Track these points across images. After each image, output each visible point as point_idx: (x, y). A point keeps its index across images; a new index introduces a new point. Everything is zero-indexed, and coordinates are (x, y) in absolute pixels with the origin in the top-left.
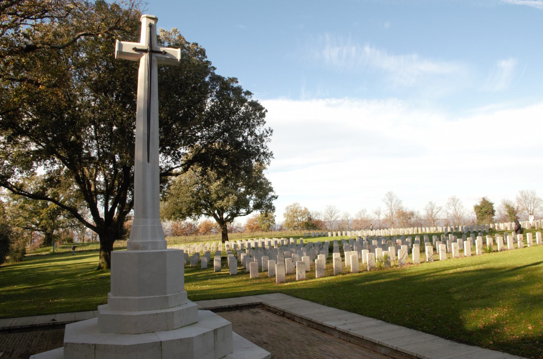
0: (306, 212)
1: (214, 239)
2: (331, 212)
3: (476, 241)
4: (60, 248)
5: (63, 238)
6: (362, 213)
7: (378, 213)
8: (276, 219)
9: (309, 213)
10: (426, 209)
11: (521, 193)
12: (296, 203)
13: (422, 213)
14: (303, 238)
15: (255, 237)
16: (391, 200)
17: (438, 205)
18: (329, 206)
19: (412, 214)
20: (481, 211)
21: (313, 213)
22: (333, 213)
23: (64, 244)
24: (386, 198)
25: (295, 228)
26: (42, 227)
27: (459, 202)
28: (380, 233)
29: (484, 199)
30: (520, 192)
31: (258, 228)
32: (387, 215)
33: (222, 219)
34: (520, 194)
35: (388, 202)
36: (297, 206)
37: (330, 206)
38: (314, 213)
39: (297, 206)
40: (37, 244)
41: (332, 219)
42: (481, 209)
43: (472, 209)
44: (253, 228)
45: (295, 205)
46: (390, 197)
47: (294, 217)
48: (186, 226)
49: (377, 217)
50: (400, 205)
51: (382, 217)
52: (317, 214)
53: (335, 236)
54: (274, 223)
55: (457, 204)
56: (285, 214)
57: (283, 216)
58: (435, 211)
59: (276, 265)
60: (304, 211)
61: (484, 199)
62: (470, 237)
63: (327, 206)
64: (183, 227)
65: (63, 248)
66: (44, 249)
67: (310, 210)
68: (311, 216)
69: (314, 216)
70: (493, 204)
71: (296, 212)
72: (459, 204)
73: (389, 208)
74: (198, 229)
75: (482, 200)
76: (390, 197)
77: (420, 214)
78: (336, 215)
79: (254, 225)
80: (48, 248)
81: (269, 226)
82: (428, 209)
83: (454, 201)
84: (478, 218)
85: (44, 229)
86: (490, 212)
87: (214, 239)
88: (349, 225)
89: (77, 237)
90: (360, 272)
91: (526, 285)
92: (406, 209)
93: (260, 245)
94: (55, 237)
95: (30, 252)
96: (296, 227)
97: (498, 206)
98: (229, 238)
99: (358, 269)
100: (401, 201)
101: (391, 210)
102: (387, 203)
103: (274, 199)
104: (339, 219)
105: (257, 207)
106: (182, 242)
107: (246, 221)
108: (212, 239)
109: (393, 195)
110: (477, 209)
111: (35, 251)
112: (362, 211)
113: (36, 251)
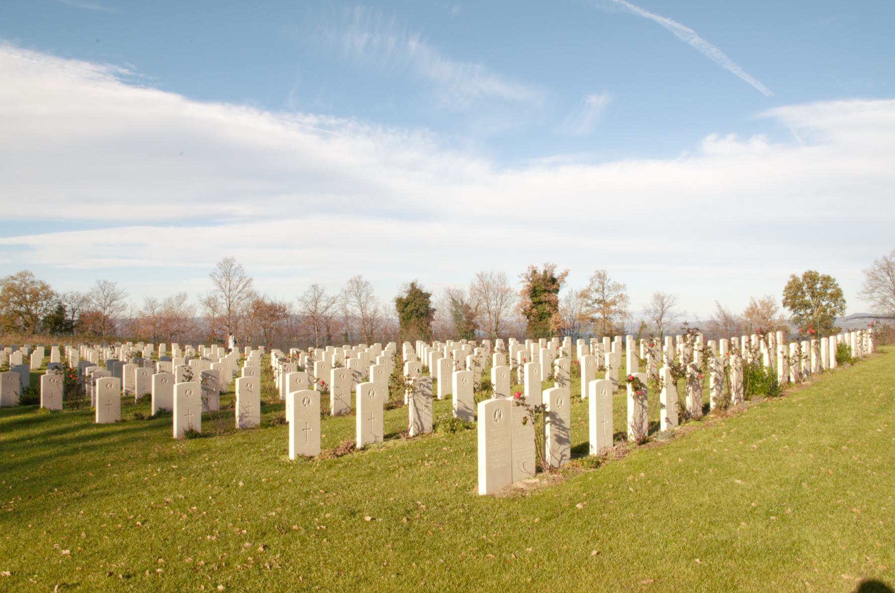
11: (481, 277)
14: (731, 387)
16: (228, 275)
20: (405, 309)
29: (413, 285)
30: (478, 276)
34: (478, 279)
43: (393, 306)
59: (153, 376)
75: (409, 288)
77: (293, 309)
83: (358, 287)
97: (438, 301)
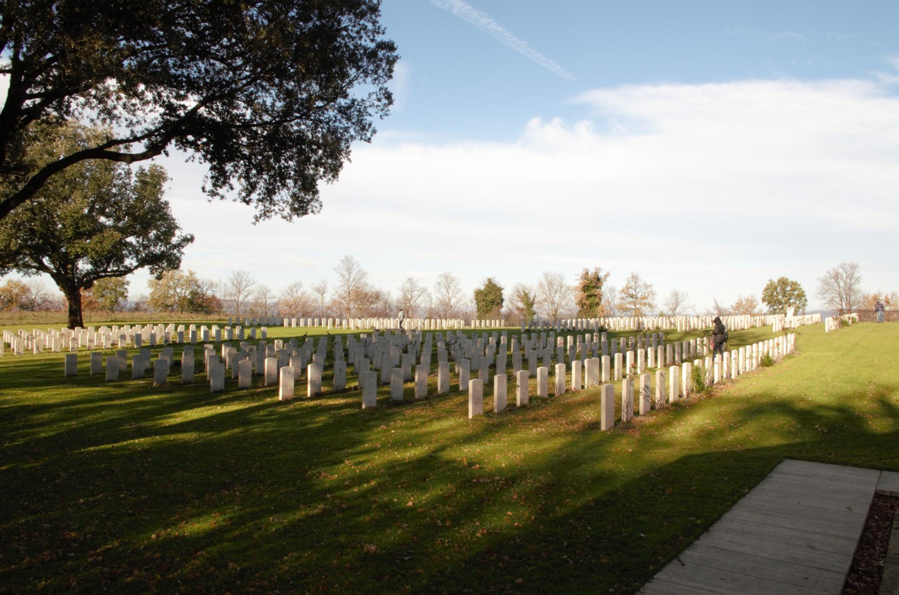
2: (240, 283)
7: (322, 291)
13: (394, 294)
16: (349, 270)
17: (421, 284)
19: (377, 296)
22: (244, 284)
27: (454, 283)
28: (424, 324)
29: (489, 280)
42: (486, 295)
43: (471, 295)
46: (348, 264)
49: (315, 295)
51: (328, 299)
52: (211, 285)
55: (452, 286)
58: (416, 293)
61: (489, 280)
70: (502, 289)
72: (455, 286)
76: (348, 264)
83: (448, 281)
84: (479, 309)
86: (498, 301)
91: (548, 484)
102: (342, 276)
110: (480, 295)
112: (295, 285)
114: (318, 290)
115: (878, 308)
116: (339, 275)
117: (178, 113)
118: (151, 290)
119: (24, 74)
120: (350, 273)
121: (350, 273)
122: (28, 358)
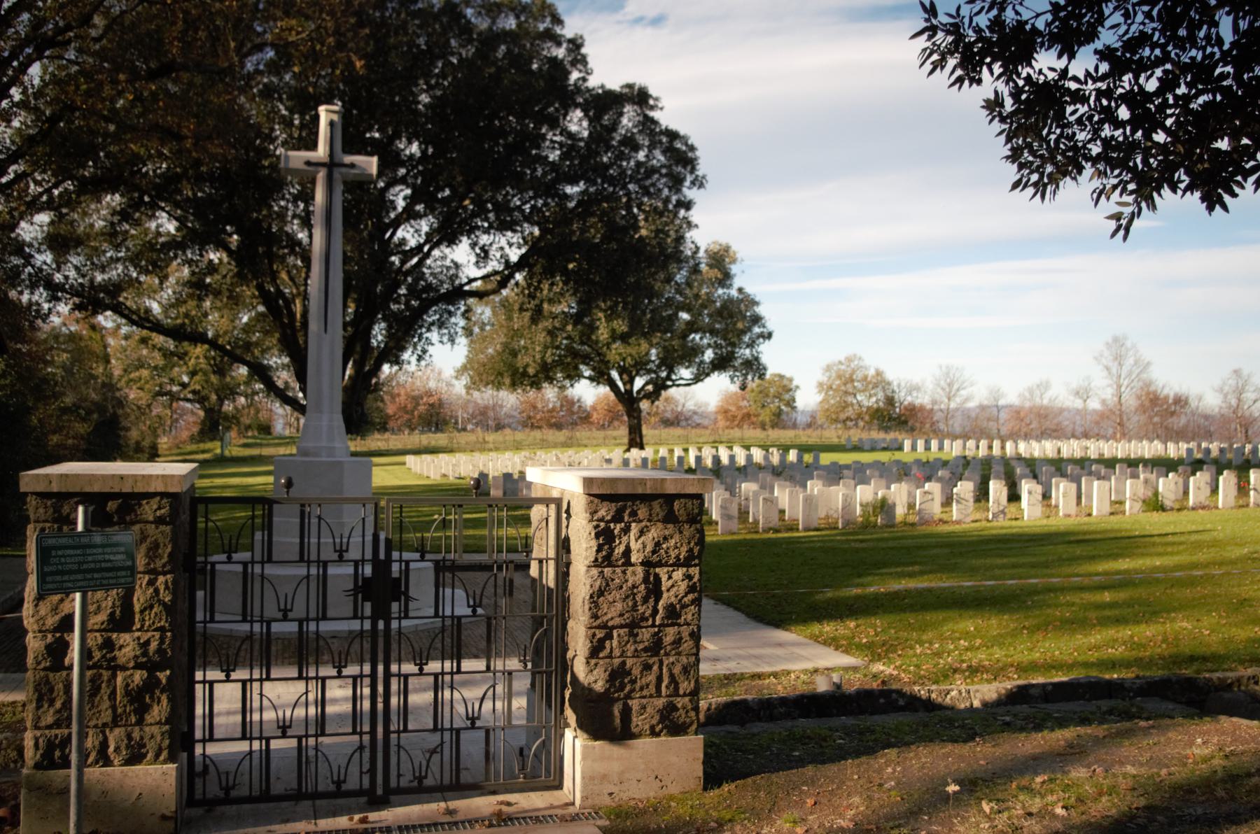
0: (879, 381)
1: (618, 441)
2: (950, 385)
3: (1221, 478)
4: (239, 446)
5: (246, 421)
6: (1038, 392)
7: (1083, 393)
8: (798, 398)
9: (889, 384)
10: (1221, 390)
12: (855, 355)
15: (721, 442)
16: (1119, 359)
18: (944, 369)
19: (1180, 401)
21: (899, 386)
22: (955, 387)
23: (248, 437)
24: (1106, 353)
25: (849, 423)
26: (194, 392)
31: (748, 416)
32: (1103, 402)
33: (629, 392)
35: (1110, 364)
36: (856, 363)
37: (947, 367)
38: (903, 384)
39: (856, 363)
40: (185, 435)
41: (953, 405)
44: (734, 417)
45: (849, 360)
47: (846, 393)
48: (558, 404)
49: (1078, 404)
50: (1144, 376)
53: (923, 450)
54: (794, 408)
56: (820, 385)
57: (816, 390)
60: (873, 377)
62: (812, 479)
63: (941, 367)
64: (551, 406)
65: (245, 446)
66: (202, 446)
67: (890, 375)
68: (893, 392)
69: (902, 394)
71: (852, 381)
73: (1110, 382)
74: (589, 413)
76: (1118, 348)
78: (963, 392)
79: (739, 408)
80: (209, 445)
81: (779, 414)
82: (1226, 389)
85: (200, 399)
87: (618, 441)
88: (1001, 421)
89: (281, 421)
90: (817, 529)
92: (1163, 387)
93: (709, 462)
94: (227, 418)
95: (168, 453)
96: (851, 420)
98: (645, 440)
99: (815, 525)
100: (1149, 364)
101: (1119, 387)
103: (761, 340)
104: (971, 405)
105: (721, 364)
106: (535, 444)
107: (719, 398)
108: (613, 441)
109: (1128, 344)
111: (179, 451)
113: (182, 451)
114: (1077, 393)
115: (675, 206)
116: (1101, 367)
117: (1226, 139)
118: (819, 398)
119: (1054, 110)
120: (1120, 365)
121: (1120, 365)
122: (444, 481)
